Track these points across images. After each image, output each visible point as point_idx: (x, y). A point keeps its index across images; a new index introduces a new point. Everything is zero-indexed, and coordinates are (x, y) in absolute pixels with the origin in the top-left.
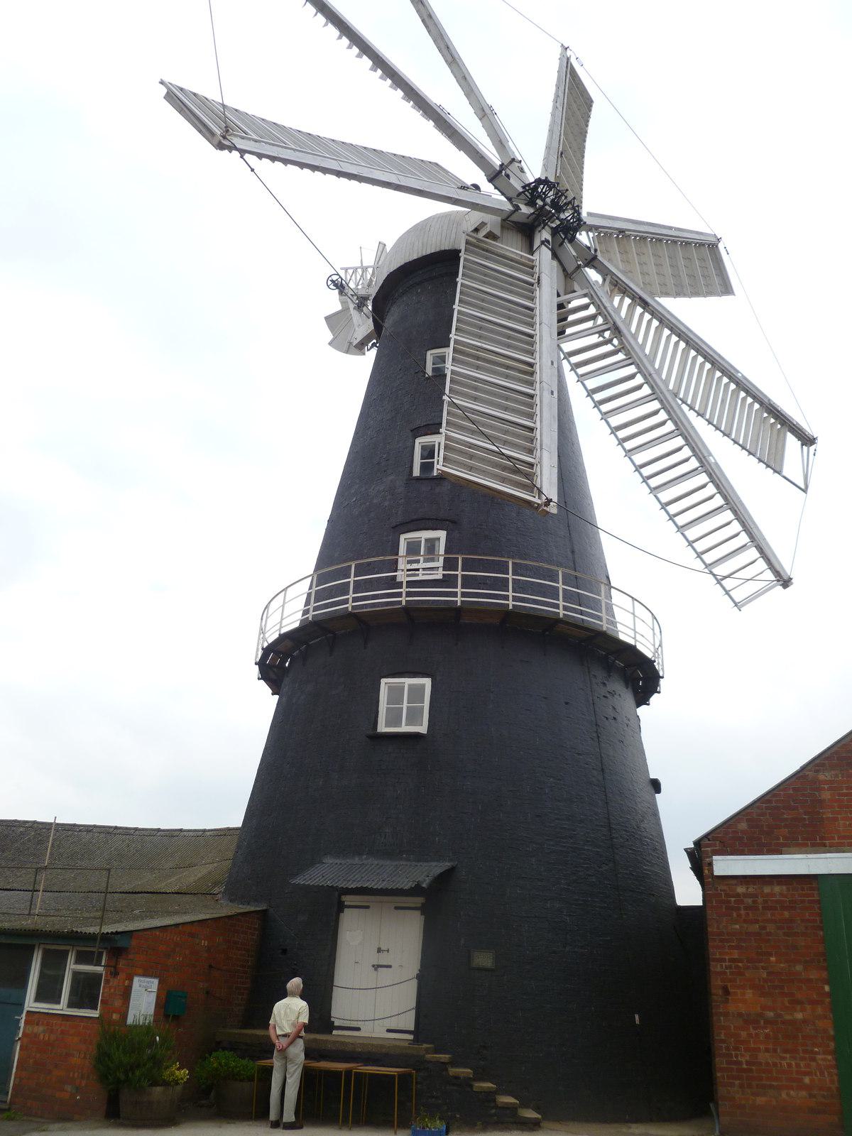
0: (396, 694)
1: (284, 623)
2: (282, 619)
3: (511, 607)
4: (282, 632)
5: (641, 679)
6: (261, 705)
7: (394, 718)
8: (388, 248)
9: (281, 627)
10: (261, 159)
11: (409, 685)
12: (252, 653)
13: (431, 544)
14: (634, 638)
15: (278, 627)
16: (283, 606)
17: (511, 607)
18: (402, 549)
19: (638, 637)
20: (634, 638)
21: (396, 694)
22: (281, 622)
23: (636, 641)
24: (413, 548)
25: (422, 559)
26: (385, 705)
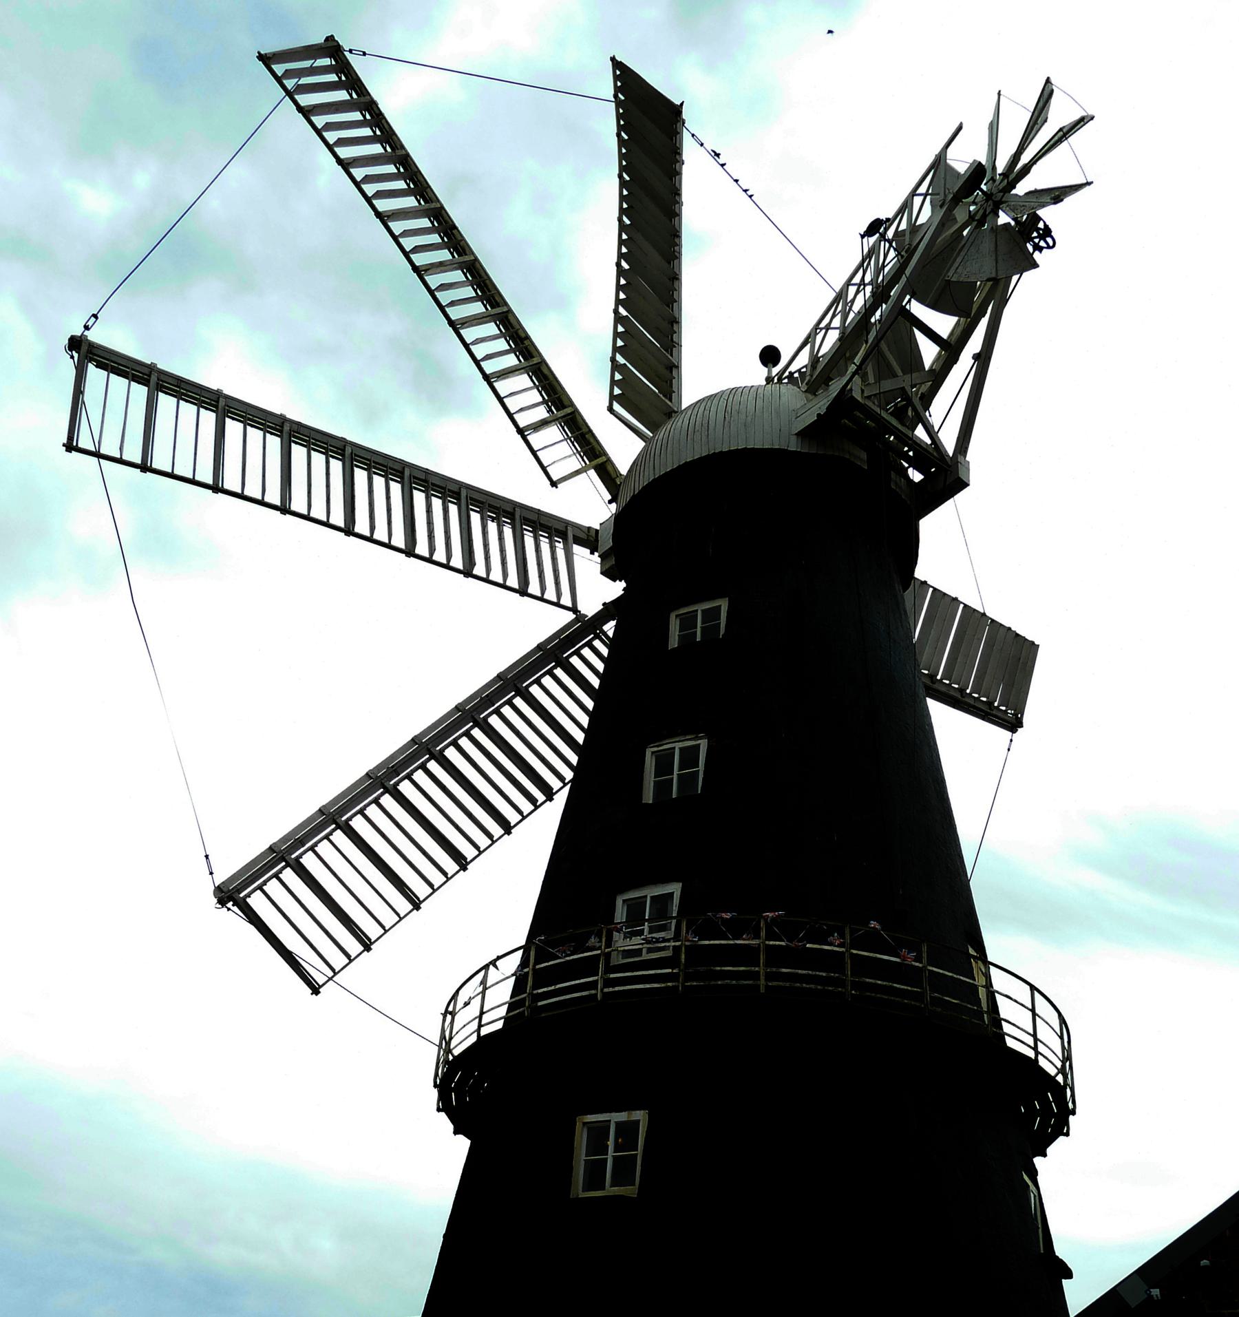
0: (598, 1134)
1: (485, 1019)
2: (482, 1013)
3: (762, 990)
4: (484, 1031)
5: (1054, 1115)
6: (438, 1158)
7: (595, 1176)
8: (955, 733)
9: (480, 1026)
10: (604, 604)
11: (617, 1124)
12: (423, 1066)
13: (662, 902)
14: (1035, 1048)
15: (475, 1025)
16: (485, 989)
17: (762, 990)
18: (620, 914)
19: (1041, 1048)
20: (1035, 1048)
21: (598, 1134)
22: (480, 1017)
23: (1037, 1053)
24: (635, 909)
25: (646, 927)
26: (584, 1157)
